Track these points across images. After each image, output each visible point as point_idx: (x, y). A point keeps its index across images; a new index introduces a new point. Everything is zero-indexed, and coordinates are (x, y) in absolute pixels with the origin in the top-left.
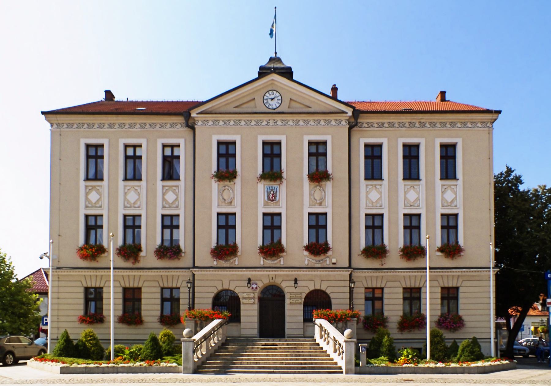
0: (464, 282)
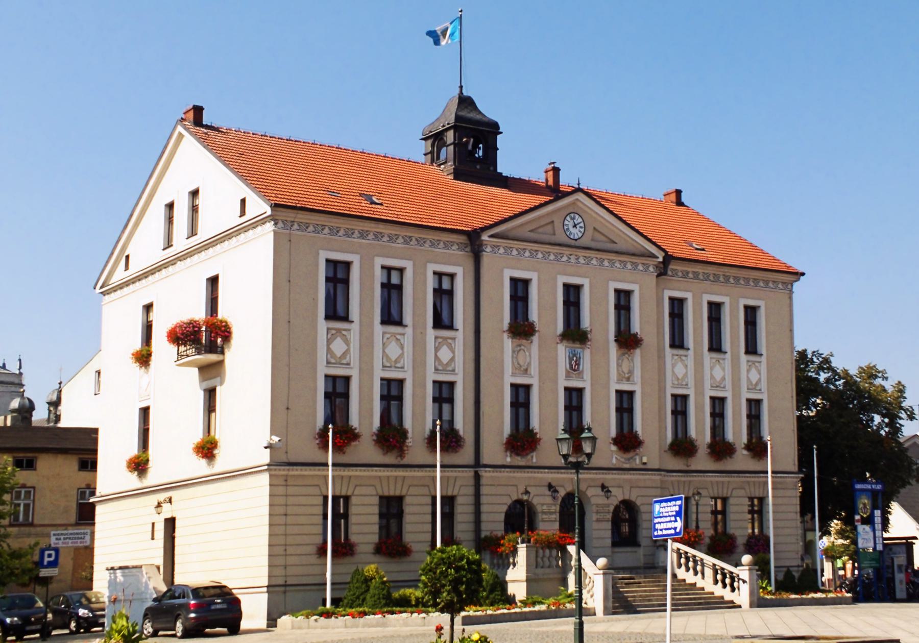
0: (358, 488)
